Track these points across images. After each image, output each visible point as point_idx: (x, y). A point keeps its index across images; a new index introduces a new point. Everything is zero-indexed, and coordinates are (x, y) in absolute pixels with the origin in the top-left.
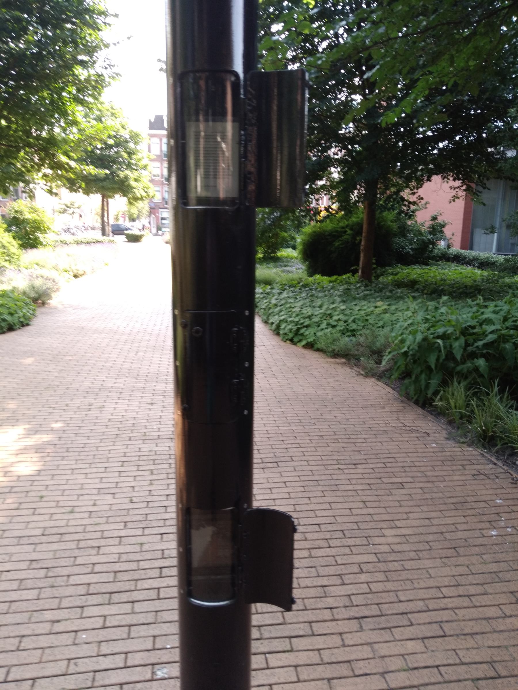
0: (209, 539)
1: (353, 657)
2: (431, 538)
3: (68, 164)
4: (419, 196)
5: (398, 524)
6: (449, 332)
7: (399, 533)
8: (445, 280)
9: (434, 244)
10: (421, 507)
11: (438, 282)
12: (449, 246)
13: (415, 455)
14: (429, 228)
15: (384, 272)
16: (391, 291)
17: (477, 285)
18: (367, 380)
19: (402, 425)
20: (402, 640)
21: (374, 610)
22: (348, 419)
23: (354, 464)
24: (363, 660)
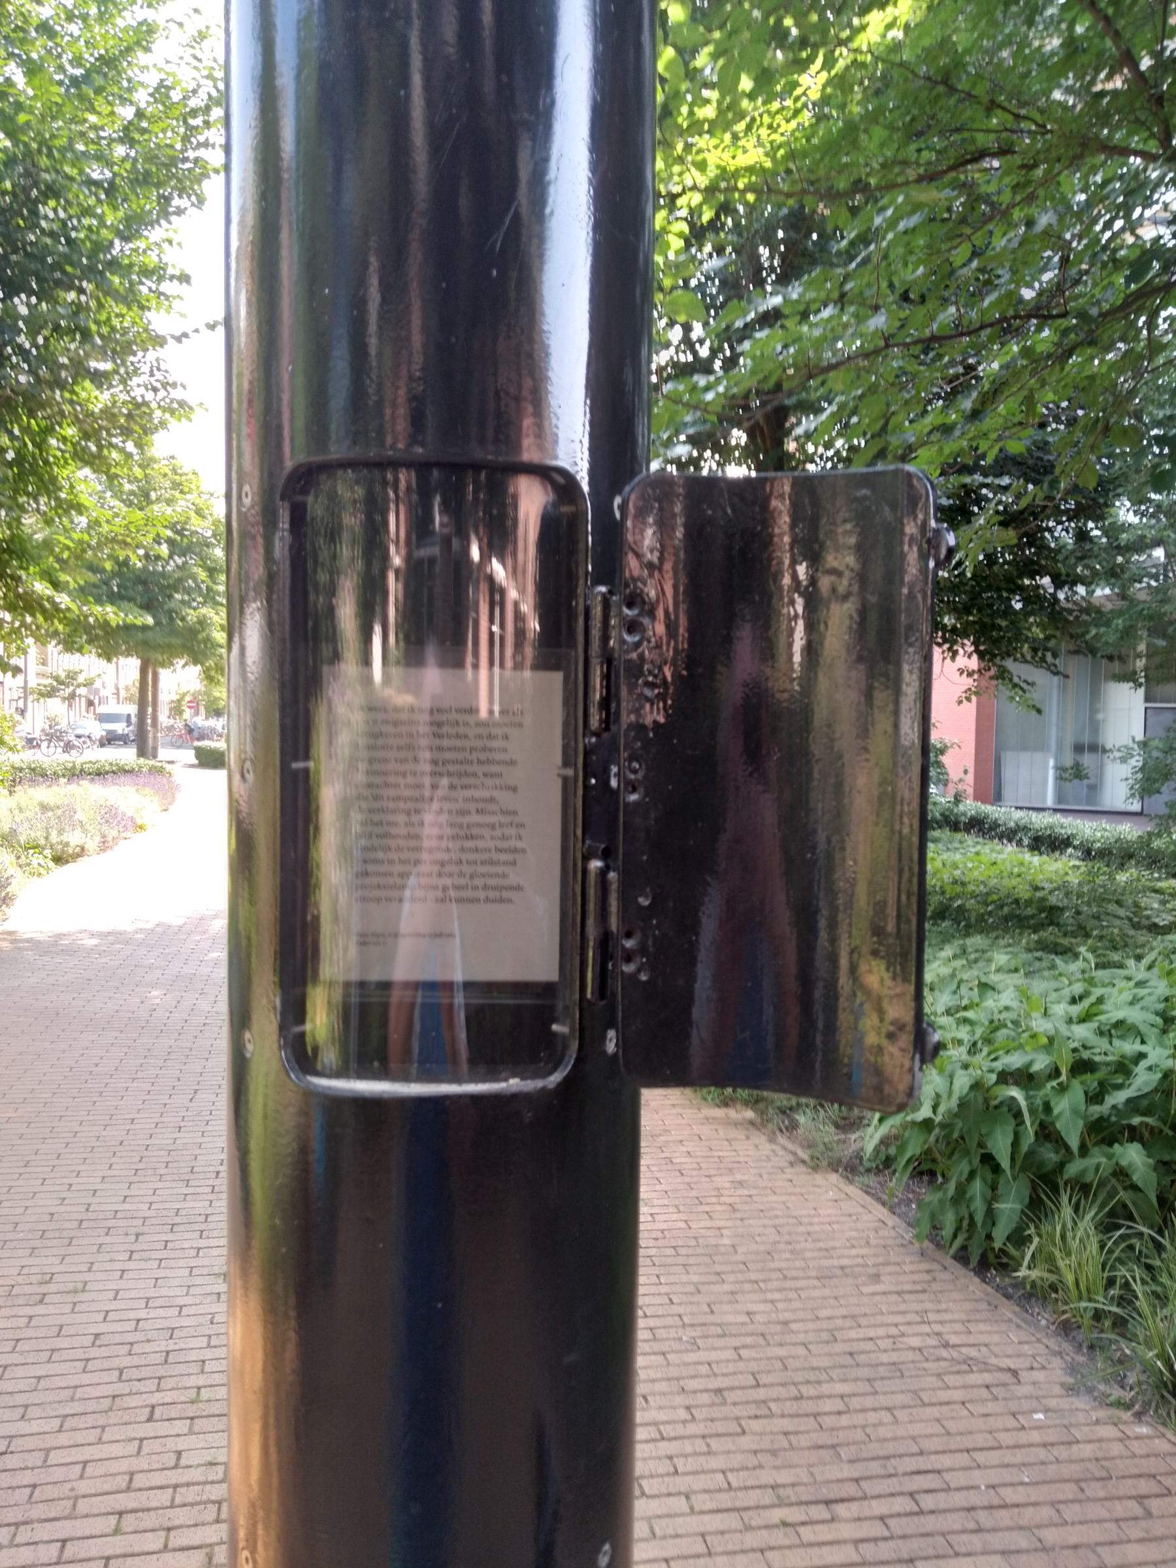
3: (50, 599)
8: (963, 884)
11: (948, 888)
17: (1044, 899)
18: (819, 1178)
22: (786, 1323)
23: (828, 1503)
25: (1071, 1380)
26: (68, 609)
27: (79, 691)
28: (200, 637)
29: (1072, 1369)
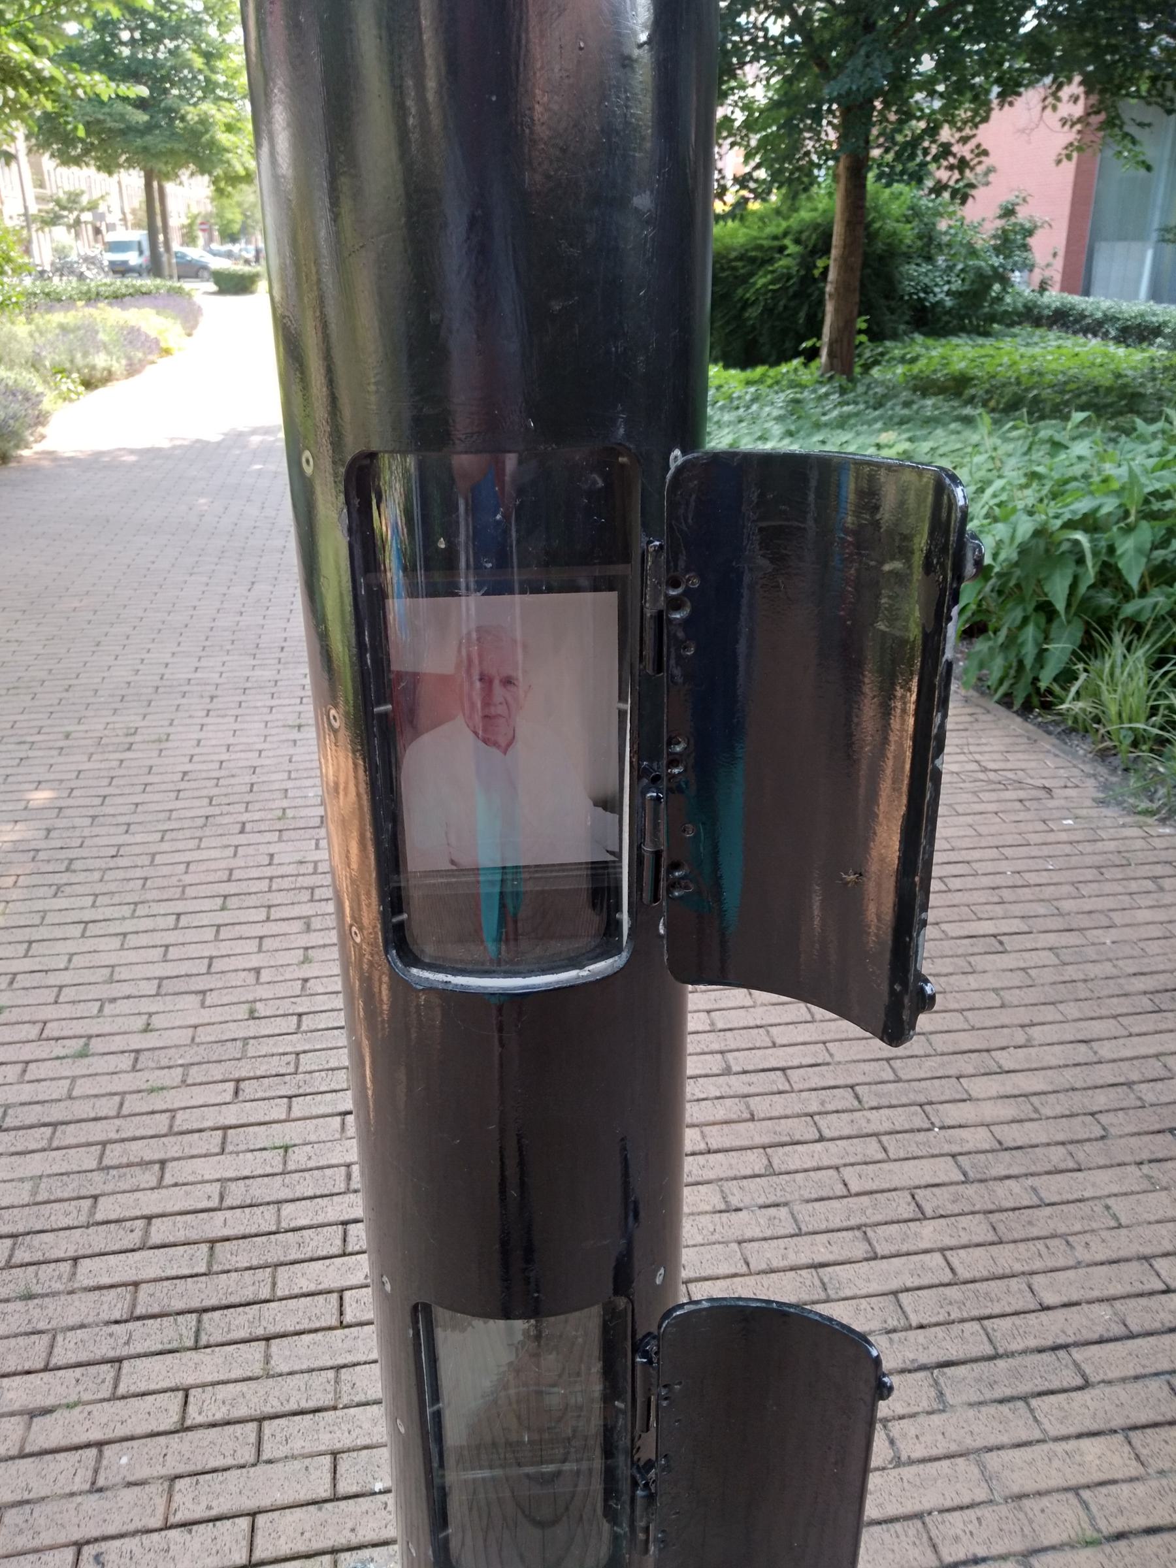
0: (506, 1357)
1: (929, 1500)
2: (1101, 1100)
3: (30, 67)
4: (978, 146)
5: (1006, 1060)
6: (1105, 510)
7: (1009, 1090)
8: (1040, 374)
9: (1005, 281)
10: (1061, 1007)
11: (1024, 379)
13: (1023, 851)
14: (994, 237)
15: (882, 354)
17: (1125, 386)
19: (974, 766)
20: (1066, 1438)
21: (972, 1341)
24: (961, 1508)
25: (1101, 795)
26: (53, 79)
28: (204, 140)
29: (1105, 787)
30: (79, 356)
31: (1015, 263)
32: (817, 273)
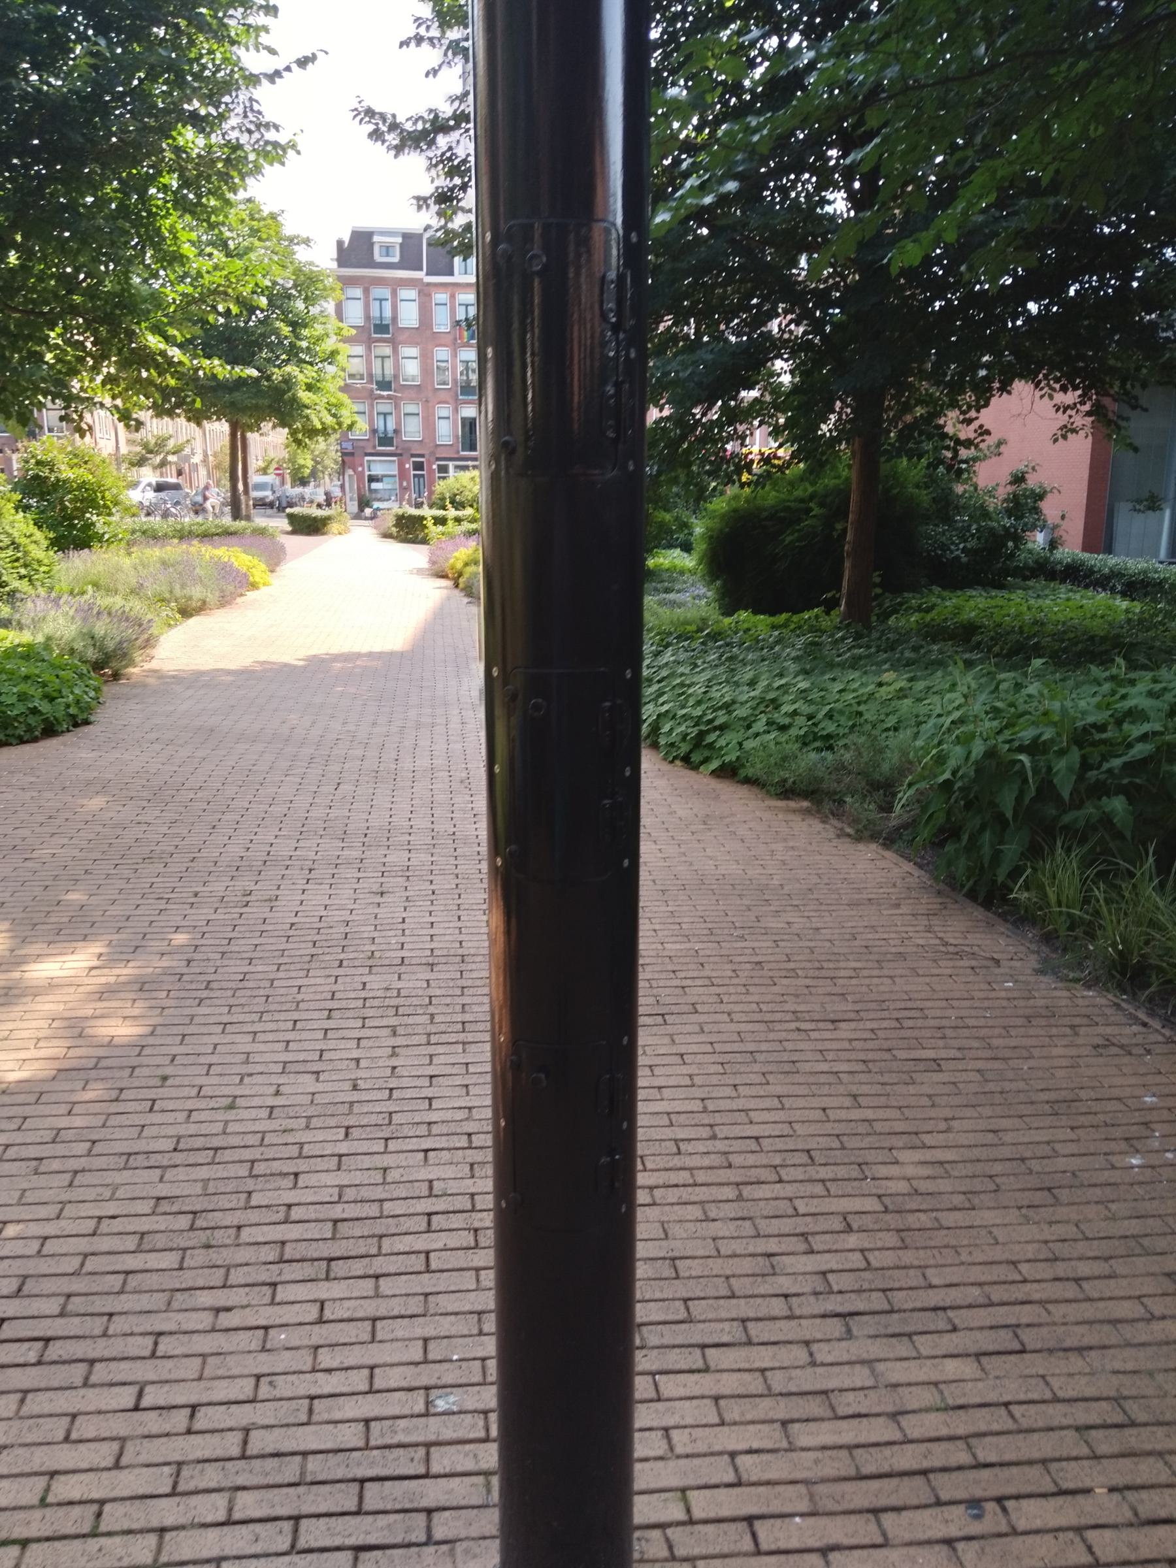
2: (998, 1168)
3: (163, 353)
4: (981, 426)
5: (928, 1139)
6: (1044, 738)
8: (1043, 624)
9: (1018, 539)
11: (1026, 629)
12: (1053, 544)
14: (1005, 500)
15: (901, 604)
16: (915, 649)
18: (861, 846)
26: (180, 363)
27: (171, 458)
30: (177, 587)
31: (1026, 524)
32: (835, 534)
